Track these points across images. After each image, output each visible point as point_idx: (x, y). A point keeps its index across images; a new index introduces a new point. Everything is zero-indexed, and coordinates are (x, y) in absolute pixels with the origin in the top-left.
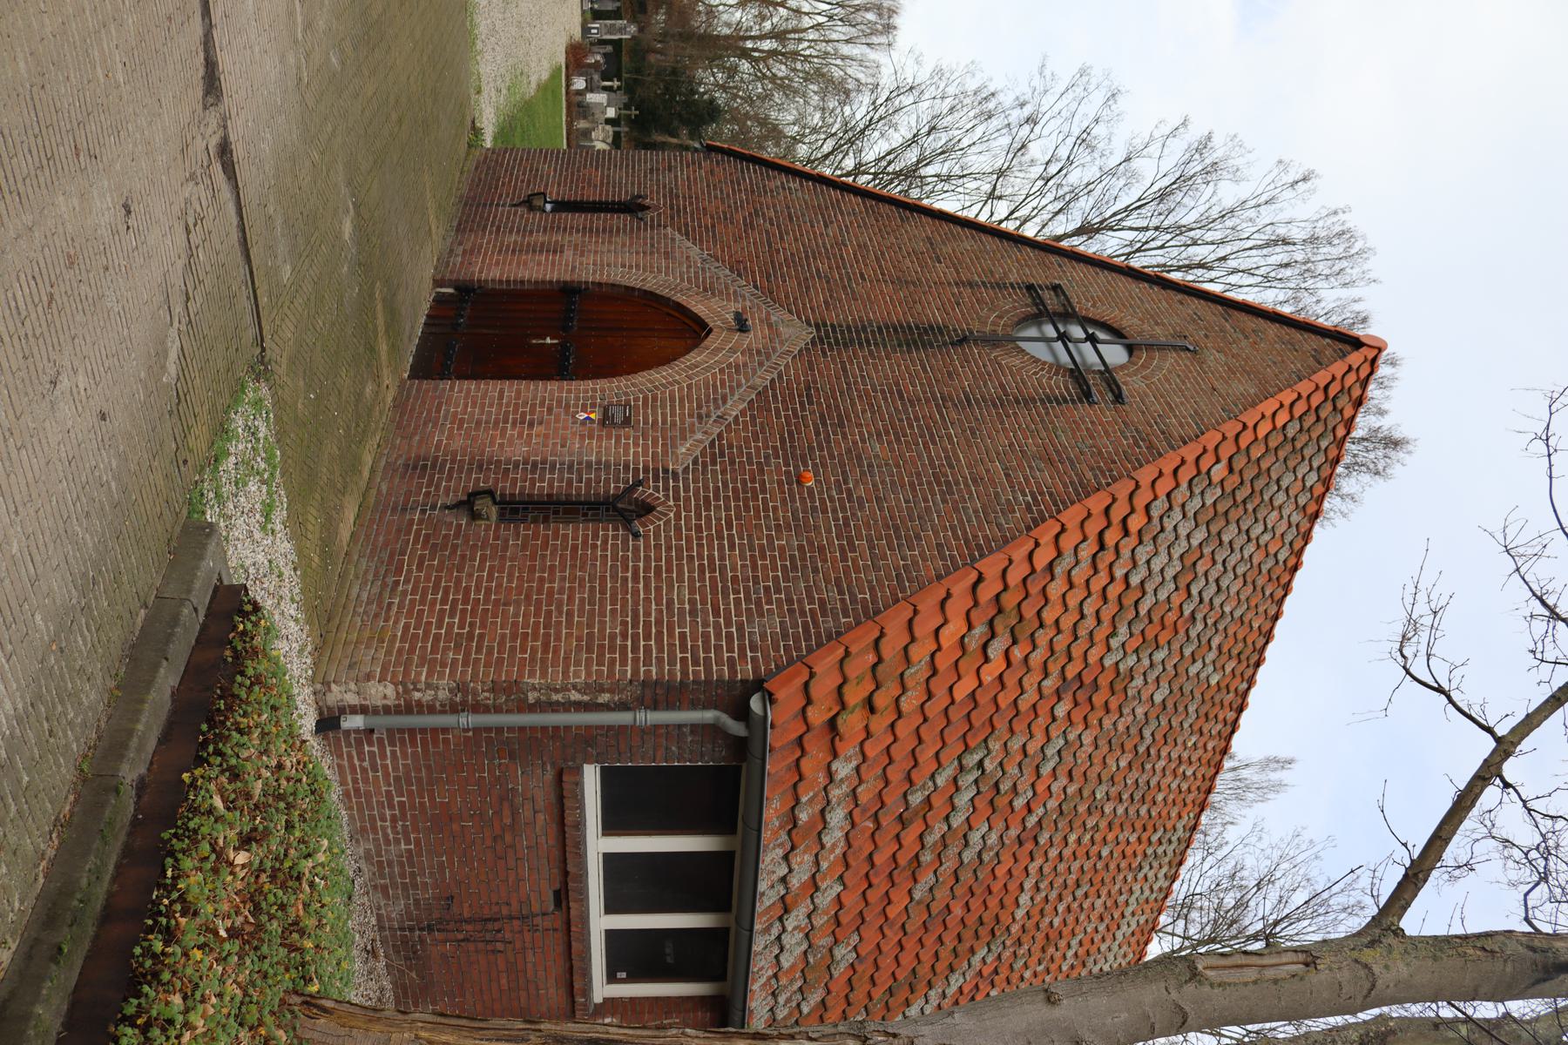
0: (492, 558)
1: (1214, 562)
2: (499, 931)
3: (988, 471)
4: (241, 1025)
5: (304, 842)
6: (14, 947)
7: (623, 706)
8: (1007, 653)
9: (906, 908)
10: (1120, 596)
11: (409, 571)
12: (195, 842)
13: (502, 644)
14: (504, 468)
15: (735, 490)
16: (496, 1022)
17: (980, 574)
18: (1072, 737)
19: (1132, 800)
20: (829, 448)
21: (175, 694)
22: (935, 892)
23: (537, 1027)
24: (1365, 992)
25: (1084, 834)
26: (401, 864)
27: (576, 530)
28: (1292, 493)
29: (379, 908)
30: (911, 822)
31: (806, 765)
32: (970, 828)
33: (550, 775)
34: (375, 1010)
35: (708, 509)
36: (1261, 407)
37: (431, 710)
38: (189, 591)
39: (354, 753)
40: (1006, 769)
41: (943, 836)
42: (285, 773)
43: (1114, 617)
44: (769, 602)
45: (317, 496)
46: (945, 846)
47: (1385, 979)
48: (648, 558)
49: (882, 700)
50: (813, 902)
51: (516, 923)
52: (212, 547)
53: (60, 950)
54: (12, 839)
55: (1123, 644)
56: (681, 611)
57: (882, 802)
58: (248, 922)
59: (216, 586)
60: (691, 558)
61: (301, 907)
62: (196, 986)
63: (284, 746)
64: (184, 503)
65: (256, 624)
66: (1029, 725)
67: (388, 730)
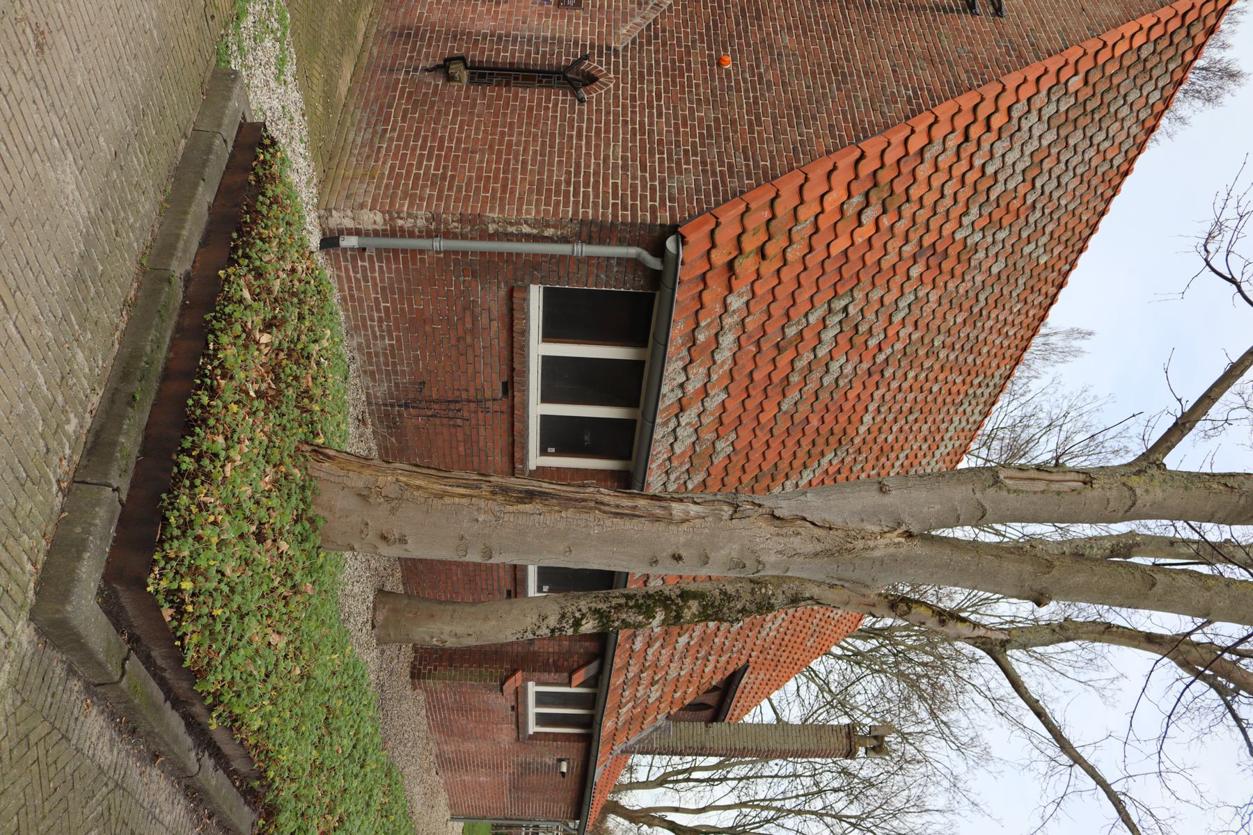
0: (463, 114)
1: (1059, 162)
2: (459, 410)
3: (878, 66)
4: (267, 462)
5: (312, 331)
6: (101, 394)
7: (564, 240)
8: (877, 220)
9: (775, 416)
10: (976, 182)
11: (395, 122)
12: (230, 324)
13: (469, 184)
14: (474, 39)
15: (665, 68)
16: (456, 474)
17: (863, 152)
18: (921, 294)
19: (963, 350)
20: (747, 37)
21: (210, 209)
22: (799, 406)
23: (488, 479)
24: (1127, 507)
25: (920, 372)
26: (385, 355)
27: (532, 94)
28: (1135, 108)
29: (368, 388)
30: (786, 349)
31: (707, 296)
32: (832, 359)
33: (503, 292)
34: (366, 459)
35: (642, 83)
36: (1122, 29)
37: (411, 234)
38: (219, 126)
39: (350, 267)
40: (866, 314)
41: (809, 363)
42: (298, 275)
43: (968, 199)
44: (687, 163)
45: (320, 55)
46: (811, 371)
47: (1143, 499)
48: (590, 120)
49: (773, 249)
50: (703, 405)
51: (472, 405)
52: (236, 91)
53: (134, 397)
54: (94, 313)
55: (973, 223)
56: (615, 166)
57: (764, 332)
58: (271, 388)
59: (241, 123)
60: (625, 122)
61: (310, 379)
62: (234, 431)
63: (296, 255)
64: (213, 52)
65: (273, 156)
66: (888, 281)
67: (377, 249)
